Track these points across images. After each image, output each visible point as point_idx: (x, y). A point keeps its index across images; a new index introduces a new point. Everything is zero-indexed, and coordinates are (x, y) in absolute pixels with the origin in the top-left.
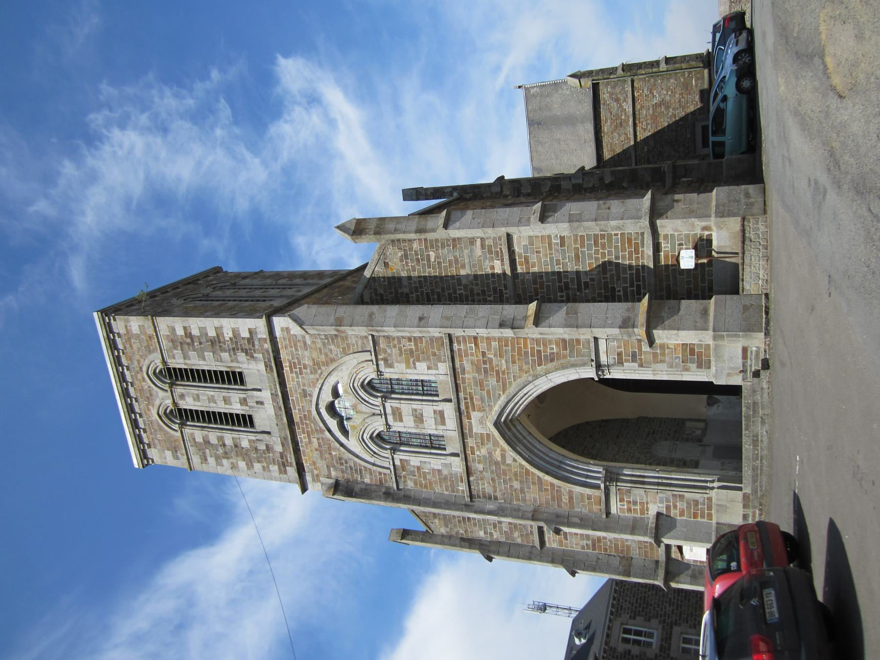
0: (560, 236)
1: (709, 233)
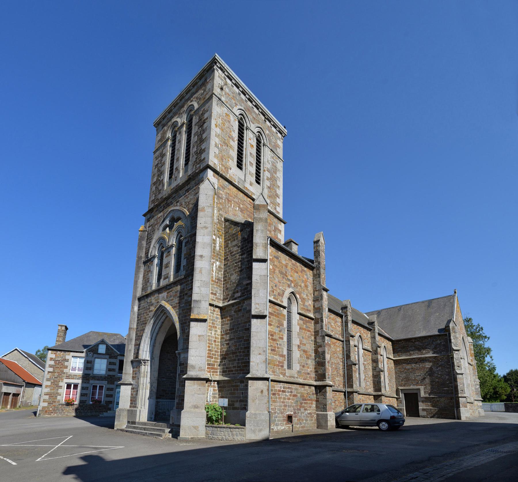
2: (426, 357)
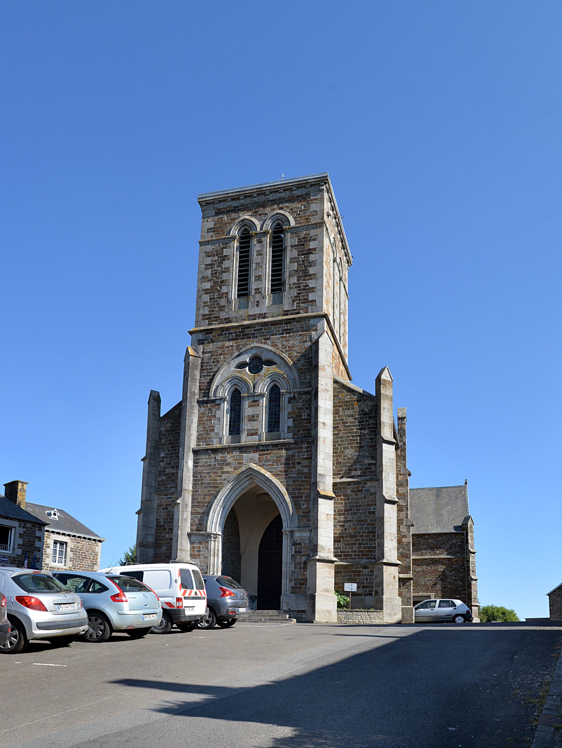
0: (375, 512)
2: (440, 559)
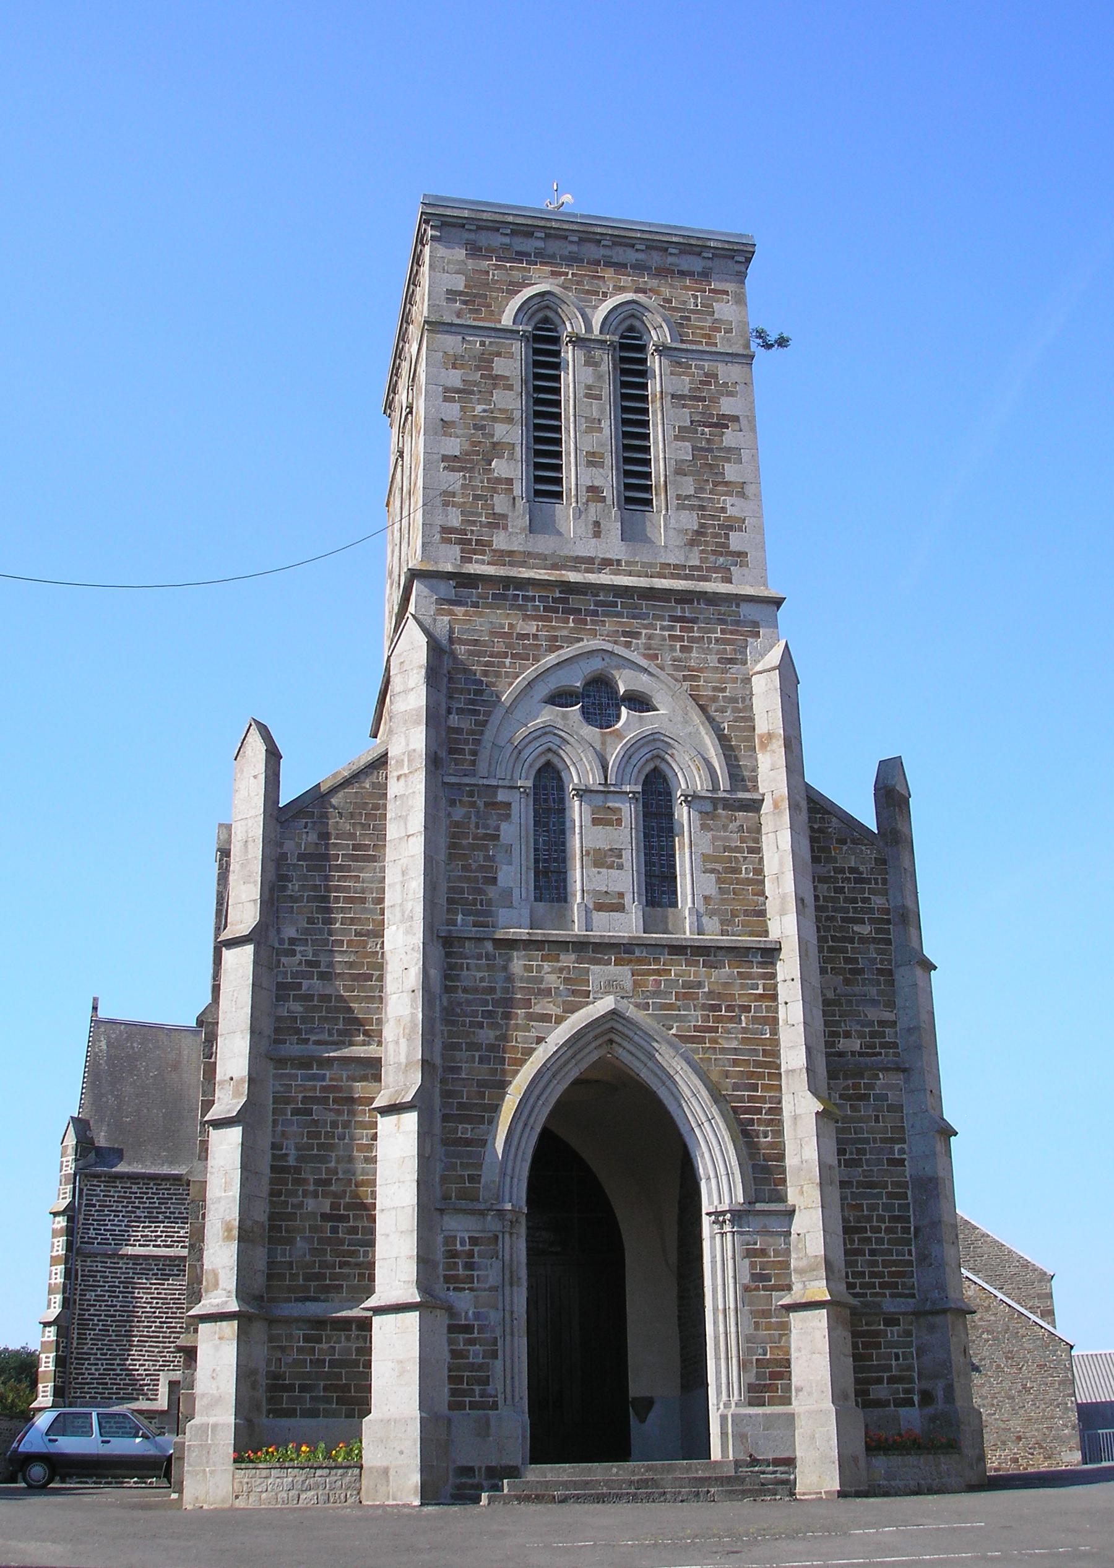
1: (916, 1403)
